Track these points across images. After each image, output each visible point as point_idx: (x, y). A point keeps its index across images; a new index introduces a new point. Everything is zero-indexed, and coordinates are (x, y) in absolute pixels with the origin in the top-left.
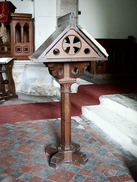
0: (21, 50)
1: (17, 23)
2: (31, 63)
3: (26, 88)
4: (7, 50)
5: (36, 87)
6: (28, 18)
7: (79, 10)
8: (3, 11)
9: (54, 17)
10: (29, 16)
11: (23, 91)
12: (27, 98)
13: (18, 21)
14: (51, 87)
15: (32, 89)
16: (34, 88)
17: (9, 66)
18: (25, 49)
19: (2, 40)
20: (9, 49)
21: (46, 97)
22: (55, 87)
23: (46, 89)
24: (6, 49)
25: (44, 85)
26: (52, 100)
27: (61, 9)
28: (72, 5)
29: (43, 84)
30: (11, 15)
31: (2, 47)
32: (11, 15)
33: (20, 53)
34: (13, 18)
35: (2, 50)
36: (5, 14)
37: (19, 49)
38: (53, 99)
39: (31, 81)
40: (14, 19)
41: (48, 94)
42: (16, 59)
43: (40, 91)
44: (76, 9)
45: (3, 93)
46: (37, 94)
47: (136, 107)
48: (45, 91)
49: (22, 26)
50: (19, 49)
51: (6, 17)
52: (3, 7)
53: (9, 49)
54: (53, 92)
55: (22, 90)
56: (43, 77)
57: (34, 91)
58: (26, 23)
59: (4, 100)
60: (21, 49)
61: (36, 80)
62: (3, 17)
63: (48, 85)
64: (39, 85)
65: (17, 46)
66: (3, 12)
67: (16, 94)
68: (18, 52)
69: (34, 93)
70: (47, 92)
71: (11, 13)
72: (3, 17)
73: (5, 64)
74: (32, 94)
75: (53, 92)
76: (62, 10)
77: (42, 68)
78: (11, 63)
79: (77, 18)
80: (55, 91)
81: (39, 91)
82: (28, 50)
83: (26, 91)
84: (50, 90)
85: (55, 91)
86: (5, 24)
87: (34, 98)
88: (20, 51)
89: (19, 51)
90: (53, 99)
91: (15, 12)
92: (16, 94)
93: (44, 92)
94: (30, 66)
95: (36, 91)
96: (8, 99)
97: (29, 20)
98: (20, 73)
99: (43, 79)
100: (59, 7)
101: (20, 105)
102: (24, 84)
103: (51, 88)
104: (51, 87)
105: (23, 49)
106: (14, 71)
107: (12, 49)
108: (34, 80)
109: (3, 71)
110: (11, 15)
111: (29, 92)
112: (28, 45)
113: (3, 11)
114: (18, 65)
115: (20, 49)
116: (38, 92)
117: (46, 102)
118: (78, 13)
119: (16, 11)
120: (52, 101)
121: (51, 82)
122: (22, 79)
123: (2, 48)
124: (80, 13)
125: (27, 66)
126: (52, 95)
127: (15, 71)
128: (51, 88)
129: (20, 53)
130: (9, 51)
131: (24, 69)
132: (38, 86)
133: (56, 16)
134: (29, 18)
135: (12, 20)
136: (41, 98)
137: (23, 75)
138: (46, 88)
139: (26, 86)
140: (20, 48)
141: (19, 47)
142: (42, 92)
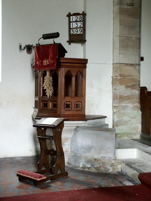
0: (72, 107)
1: (67, 72)
2: (84, 125)
3: (76, 161)
4: (52, 107)
5: (92, 159)
6: (81, 65)
7: (142, 56)
8: (51, 55)
9: (110, 64)
10: (82, 62)
11: (72, 163)
12: (81, 178)
13: (69, 69)
14: (114, 160)
15: (85, 162)
16: (89, 161)
17: (59, 130)
18: (65, 106)
19: (46, 93)
20: (55, 106)
21: (105, 175)
22: (119, 160)
23: (107, 163)
24: (50, 105)
25: (103, 157)
26: (121, 182)
27: (120, 54)
28: (133, 49)
29: (102, 155)
30: (60, 60)
31: (46, 102)
32: (61, 61)
33: (70, 110)
34: (62, 64)
35: (45, 107)
36: (53, 59)
37: (68, 106)
38: (121, 180)
39: (84, 150)
40: (64, 65)
41: (110, 171)
42: (67, 120)
43: (98, 166)
44: (138, 54)
45: (46, 168)
46: (93, 170)
47: (36, 128)
48: (106, 166)
49: (74, 74)
50: (68, 106)
51: (54, 63)
52: (50, 51)
53: (55, 106)
54: (116, 167)
55: (70, 162)
56: (102, 146)
57: (89, 166)
58: (69, 71)
59: (49, 181)
60: (72, 105)
61: (93, 150)
62: (50, 64)
63: (110, 158)
64: (96, 156)
65: (66, 102)
66: (50, 57)
67: (66, 171)
68: (66, 109)
69: (89, 168)
70: (109, 167)
71: (61, 58)
72: (50, 64)
73: (52, 128)
74: (87, 170)
75: (116, 167)
76: (120, 55)
77: (101, 132)
78: (61, 126)
79: (139, 65)
80: (119, 166)
81: (97, 165)
82: (81, 107)
83: (77, 164)
84: (112, 165)
85: (119, 166)
86: (51, 71)
87: (91, 176)
88: (70, 109)
89: (68, 109)
90: (121, 180)
91: (65, 57)
92: (66, 171)
93: (104, 168)
94: (84, 129)
95: (92, 165)
96: (55, 179)
97: (83, 67)
98: (67, 139)
99: (101, 149)
100: (117, 52)
101: (76, 191)
102: (73, 154)
103: (113, 162)
104: (114, 160)
105: (73, 105)
106: (64, 135)
107: (59, 105)
108: (89, 149)
109: (48, 136)
110: (61, 61)
111: (81, 166)
112: (80, 100)
113: (51, 55)
114: (68, 128)
115: (70, 106)
116: (96, 167)
117: (113, 185)
118: (140, 59)
119: (67, 56)
120: (121, 185)
121: (113, 152)
122: (70, 146)
123: (54, 104)
124: (142, 59)
125: (77, 129)
126: (115, 172)
127: (66, 135)
128: (114, 161)
129: (70, 110)
130: (55, 109)
131: (73, 133)
132: (95, 158)
133: (112, 62)
134: (83, 64)
135: (61, 67)
136: (102, 178)
137: (72, 141)
138: (107, 161)
139: (76, 157)
140: (69, 104)
141: (68, 103)
142: (101, 167)
